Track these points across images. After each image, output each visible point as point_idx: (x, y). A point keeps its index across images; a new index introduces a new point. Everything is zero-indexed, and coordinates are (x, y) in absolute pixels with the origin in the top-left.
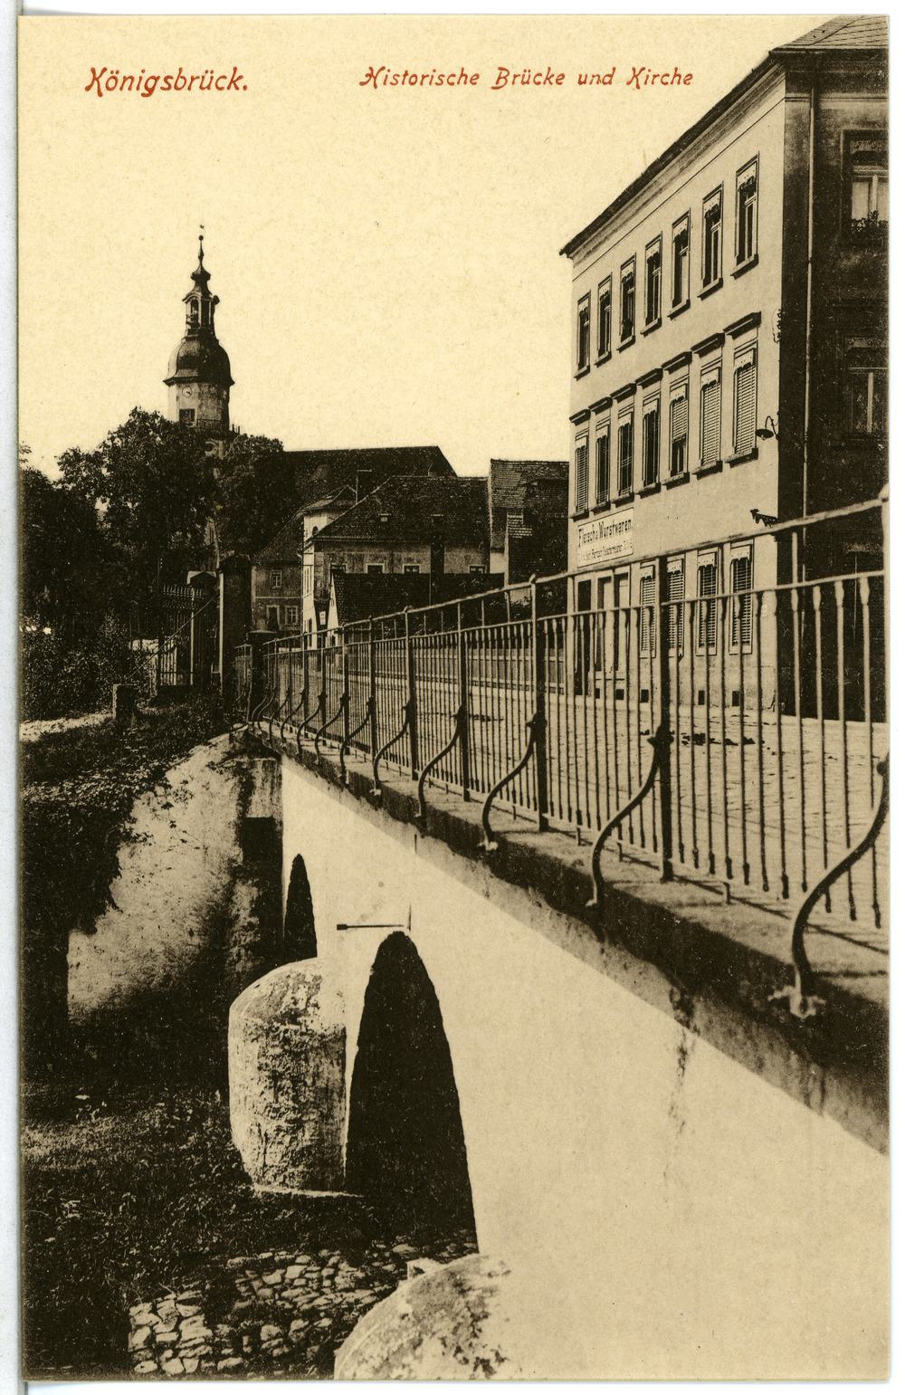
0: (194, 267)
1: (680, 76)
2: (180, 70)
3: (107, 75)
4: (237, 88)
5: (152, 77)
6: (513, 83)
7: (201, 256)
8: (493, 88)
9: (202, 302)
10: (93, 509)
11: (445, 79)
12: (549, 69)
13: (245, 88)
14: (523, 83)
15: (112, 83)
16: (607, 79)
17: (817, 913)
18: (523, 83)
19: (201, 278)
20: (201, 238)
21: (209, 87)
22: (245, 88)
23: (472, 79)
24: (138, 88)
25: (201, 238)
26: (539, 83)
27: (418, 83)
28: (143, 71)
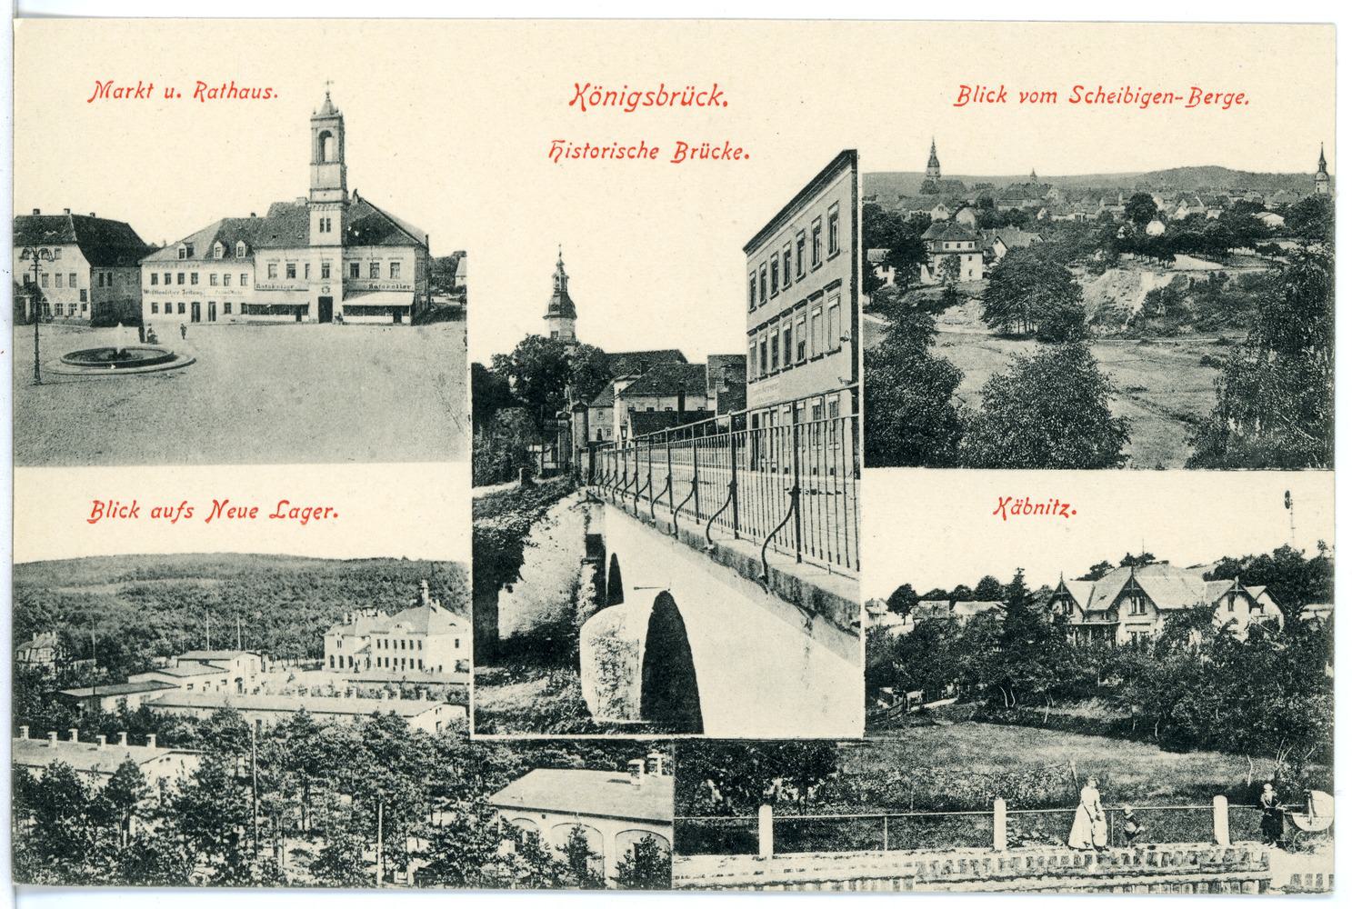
0: (557, 260)
3: (590, 91)
4: (717, 104)
5: (636, 93)
8: (955, 105)
9: (562, 279)
13: (725, 104)
15: (595, 98)
24: (621, 103)
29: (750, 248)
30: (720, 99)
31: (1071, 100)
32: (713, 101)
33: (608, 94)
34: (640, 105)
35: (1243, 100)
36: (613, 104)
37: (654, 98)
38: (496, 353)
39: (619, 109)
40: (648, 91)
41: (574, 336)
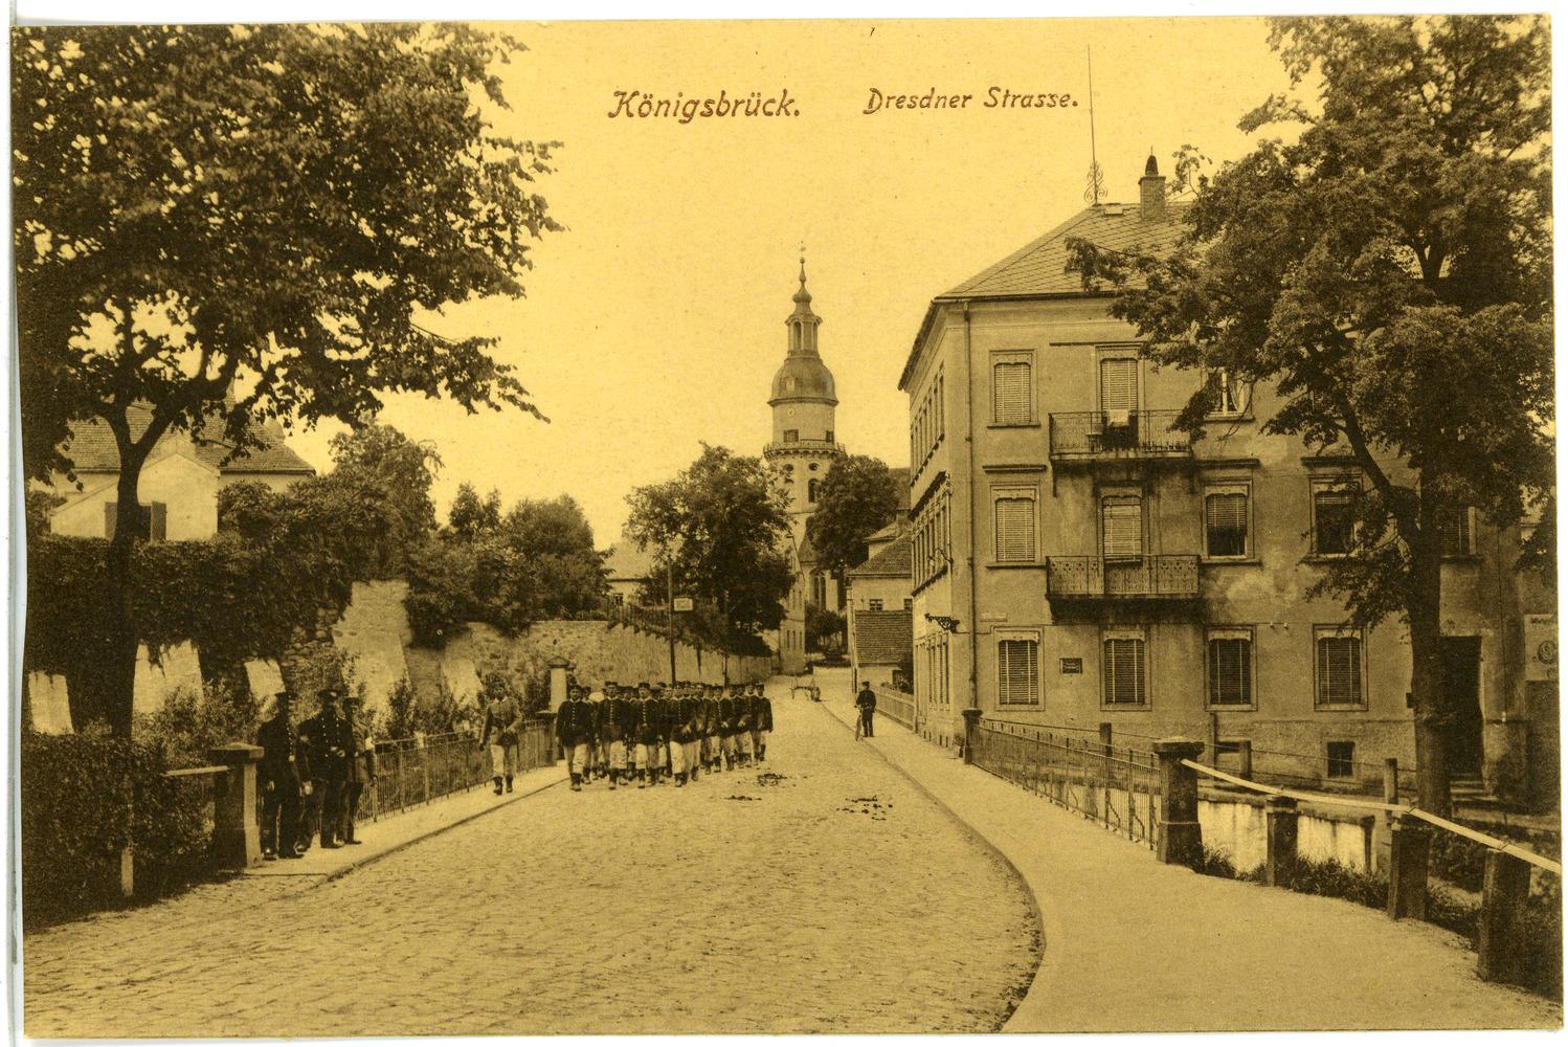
0: (796, 287)
1: (727, 102)
2: (723, 93)
3: (638, 100)
4: (788, 114)
5: (691, 102)
6: (1013, 105)
7: (803, 280)
8: (865, 112)
9: (804, 323)
10: (1066, 602)
11: (918, 102)
12: (785, 92)
13: (797, 113)
14: (748, 113)
15: (645, 109)
16: (925, 102)
17: (307, 450)
18: (748, 113)
19: (803, 299)
20: (803, 262)
21: (755, 111)
22: (797, 113)
23: (951, 102)
24: (675, 115)
25: (803, 262)
26: (770, 114)
27: (652, 113)
28: (681, 95)
29: (904, 384)
30: (791, 108)
31: (986, 104)
32: (783, 110)
33: (660, 103)
34: (697, 113)
35: (1070, 103)
36: (666, 115)
37: (714, 107)
38: (571, 495)
39: (672, 121)
40: (706, 98)
41: (830, 437)
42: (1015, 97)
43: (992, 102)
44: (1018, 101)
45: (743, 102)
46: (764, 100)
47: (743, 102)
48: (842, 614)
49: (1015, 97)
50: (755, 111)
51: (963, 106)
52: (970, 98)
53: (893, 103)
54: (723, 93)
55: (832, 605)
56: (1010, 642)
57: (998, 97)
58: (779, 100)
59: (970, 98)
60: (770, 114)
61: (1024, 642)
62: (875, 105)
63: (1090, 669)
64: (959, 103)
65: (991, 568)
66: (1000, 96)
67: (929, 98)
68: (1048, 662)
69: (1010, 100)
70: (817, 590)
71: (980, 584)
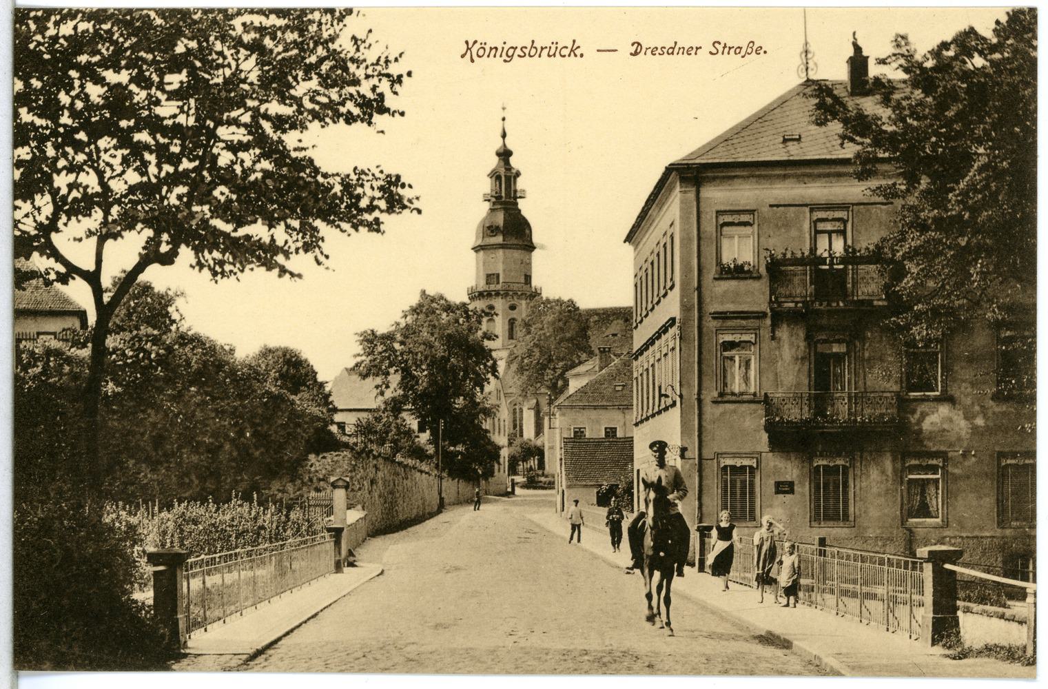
0: (498, 144)
1: (535, 48)
2: (533, 42)
3: (477, 46)
4: (576, 55)
5: (512, 48)
6: (729, 53)
7: (504, 136)
13: (582, 55)
16: (670, 51)
19: (505, 155)
24: (501, 56)
26: (564, 56)
31: (711, 53)
33: (491, 49)
37: (527, 51)
41: (528, 278)
42: (730, 48)
43: (715, 51)
44: (732, 50)
45: (546, 47)
46: (560, 46)
47: (546, 47)
48: (539, 443)
49: (730, 48)
50: (554, 55)
51: (696, 54)
52: (700, 48)
53: (649, 52)
54: (533, 42)
55: (529, 432)
56: (731, 466)
57: (719, 48)
58: (570, 47)
59: (700, 48)
60: (564, 56)
61: (743, 468)
62: (638, 51)
63: (804, 488)
64: (693, 52)
65: (715, 402)
66: (720, 48)
67: (673, 48)
68: (764, 486)
69: (727, 50)
70: (515, 420)
71: (707, 416)
